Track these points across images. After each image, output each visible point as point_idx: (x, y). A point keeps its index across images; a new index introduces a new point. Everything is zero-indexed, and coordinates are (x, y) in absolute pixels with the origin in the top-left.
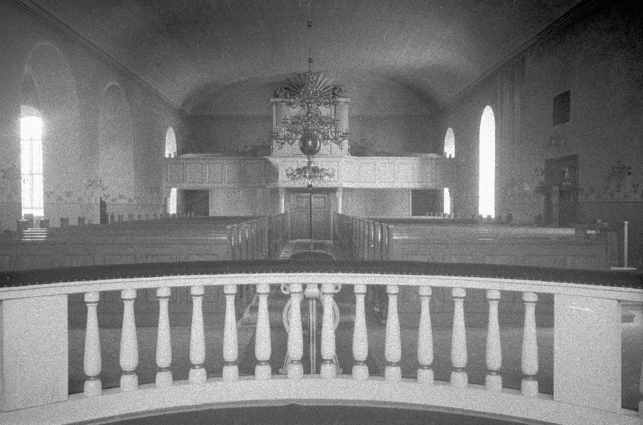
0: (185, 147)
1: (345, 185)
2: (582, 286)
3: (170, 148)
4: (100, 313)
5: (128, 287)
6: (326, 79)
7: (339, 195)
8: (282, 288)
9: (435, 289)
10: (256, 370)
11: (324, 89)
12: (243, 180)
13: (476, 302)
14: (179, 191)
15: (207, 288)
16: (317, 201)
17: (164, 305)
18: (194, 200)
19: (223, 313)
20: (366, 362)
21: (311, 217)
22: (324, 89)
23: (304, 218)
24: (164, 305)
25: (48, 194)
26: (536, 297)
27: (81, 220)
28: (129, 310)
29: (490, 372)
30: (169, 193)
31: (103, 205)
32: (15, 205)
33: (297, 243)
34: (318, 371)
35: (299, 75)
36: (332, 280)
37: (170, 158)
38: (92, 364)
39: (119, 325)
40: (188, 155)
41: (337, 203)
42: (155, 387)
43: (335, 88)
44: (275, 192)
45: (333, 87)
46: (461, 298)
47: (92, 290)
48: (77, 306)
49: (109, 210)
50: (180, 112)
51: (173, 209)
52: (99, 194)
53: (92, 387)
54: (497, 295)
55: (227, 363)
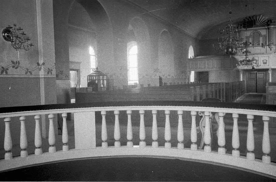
0: (197, 53)
1: (273, 67)
2: (250, 110)
3: (191, 54)
4: (270, 126)
5: (116, 110)
6: (264, 18)
7: (270, 72)
8: (199, 113)
9: (171, 111)
10: (178, 145)
11: (263, 22)
12: (223, 67)
13: (148, 115)
14: (195, 73)
15: (133, 111)
16: (260, 75)
17: (129, 117)
18: (202, 76)
19: (190, 123)
20: (119, 140)
21: (257, 82)
22: (263, 22)
23: (254, 82)
24: (129, 117)
25: (140, 75)
26: (269, 118)
27: (149, 85)
28: (117, 118)
29: (264, 154)
30: (190, 73)
31: (160, 79)
32: (125, 79)
33: (249, 94)
34: (203, 148)
35: (250, 17)
36: (222, 111)
37: (191, 59)
38: (104, 136)
39: (164, 126)
40: (198, 57)
41: (269, 75)
42: (204, 151)
43: (268, 21)
44: (238, 71)
45: (267, 21)
46: (142, 114)
47: (103, 110)
48: (98, 116)
49: (163, 82)
50: (196, 39)
51: (192, 79)
52: (158, 74)
53: (104, 145)
54: (181, 113)
55: (154, 141)
